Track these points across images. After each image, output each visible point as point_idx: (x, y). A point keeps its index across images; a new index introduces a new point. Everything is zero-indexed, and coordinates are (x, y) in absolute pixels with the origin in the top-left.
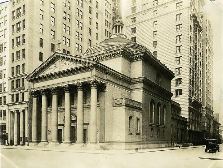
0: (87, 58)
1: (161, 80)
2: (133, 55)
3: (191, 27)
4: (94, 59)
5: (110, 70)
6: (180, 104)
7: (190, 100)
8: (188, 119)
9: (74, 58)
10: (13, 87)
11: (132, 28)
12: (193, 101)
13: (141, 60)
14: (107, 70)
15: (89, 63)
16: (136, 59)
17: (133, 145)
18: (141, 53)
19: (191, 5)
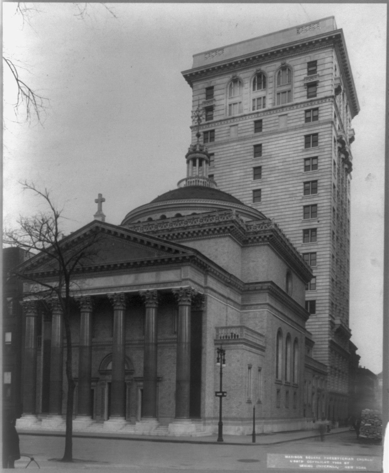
0: (148, 232)
1: (292, 286)
2: (249, 233)
3: (335, 164)
4: (164, 236)
5: (214, 268)
6: (313, 333)
7: (332, 323)
8: (328, 368)
9: (155, 242)
10: (136, 378)
11: (305, 180)
12: (337, 327)
13: (264, 245)
14: (209, 266)
15: (177, 252)
16: (253, 242)
17: (176, 353)
18: (265, 231)
19: (335, 117)
